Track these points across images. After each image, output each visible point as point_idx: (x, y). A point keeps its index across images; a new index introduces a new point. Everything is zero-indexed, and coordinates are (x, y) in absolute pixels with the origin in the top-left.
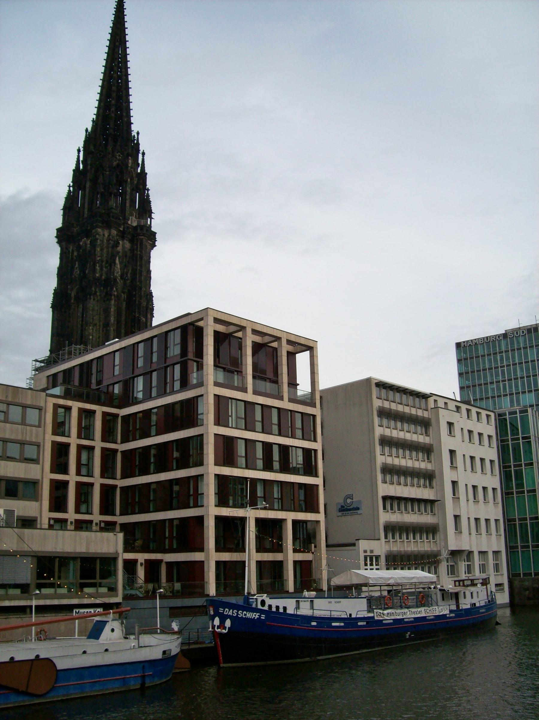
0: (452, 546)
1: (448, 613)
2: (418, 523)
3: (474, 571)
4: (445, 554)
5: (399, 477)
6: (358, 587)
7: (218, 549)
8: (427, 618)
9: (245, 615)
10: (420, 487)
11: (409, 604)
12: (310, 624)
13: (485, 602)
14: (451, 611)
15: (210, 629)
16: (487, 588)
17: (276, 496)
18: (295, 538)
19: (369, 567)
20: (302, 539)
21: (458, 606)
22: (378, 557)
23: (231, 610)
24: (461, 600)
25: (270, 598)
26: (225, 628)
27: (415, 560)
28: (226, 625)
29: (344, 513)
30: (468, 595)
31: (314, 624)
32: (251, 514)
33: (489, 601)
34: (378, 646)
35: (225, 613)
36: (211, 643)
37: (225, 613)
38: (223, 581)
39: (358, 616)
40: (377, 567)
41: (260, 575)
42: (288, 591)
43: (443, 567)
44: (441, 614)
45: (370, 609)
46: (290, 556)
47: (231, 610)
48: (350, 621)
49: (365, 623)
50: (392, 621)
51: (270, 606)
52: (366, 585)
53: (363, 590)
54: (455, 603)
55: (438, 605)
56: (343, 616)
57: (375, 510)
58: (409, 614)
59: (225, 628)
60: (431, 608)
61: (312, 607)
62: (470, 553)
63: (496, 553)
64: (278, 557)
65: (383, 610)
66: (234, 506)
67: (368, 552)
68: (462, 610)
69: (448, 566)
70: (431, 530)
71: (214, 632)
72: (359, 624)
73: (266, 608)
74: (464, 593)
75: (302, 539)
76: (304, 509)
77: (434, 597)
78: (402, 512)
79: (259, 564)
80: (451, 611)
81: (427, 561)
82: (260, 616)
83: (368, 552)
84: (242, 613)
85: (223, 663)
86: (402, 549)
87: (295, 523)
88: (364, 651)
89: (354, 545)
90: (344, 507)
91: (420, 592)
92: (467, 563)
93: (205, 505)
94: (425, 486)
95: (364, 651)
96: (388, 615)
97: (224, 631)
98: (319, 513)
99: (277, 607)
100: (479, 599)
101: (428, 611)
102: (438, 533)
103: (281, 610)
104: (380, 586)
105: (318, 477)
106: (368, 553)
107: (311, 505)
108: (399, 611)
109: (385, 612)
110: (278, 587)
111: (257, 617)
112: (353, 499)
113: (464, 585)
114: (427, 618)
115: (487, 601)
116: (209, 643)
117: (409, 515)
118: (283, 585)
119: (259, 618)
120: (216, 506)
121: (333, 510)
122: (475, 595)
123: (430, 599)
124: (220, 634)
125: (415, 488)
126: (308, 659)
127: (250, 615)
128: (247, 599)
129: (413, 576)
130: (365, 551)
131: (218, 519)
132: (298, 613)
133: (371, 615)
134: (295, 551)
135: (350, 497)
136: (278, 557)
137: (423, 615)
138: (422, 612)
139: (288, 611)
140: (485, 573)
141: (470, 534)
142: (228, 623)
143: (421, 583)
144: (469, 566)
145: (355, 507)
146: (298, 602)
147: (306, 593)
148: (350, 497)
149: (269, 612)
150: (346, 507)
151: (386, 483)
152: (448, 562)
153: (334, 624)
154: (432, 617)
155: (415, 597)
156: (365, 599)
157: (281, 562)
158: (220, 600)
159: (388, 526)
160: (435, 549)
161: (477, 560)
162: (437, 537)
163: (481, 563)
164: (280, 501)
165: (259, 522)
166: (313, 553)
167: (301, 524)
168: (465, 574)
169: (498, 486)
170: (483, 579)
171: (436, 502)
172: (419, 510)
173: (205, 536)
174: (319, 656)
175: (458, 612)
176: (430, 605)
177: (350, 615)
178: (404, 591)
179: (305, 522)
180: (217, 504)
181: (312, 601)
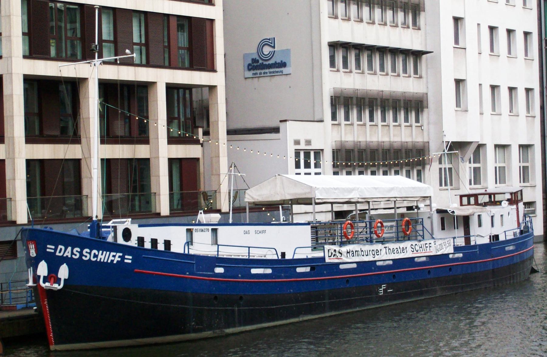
1: (452, 252)
2: (390, 92)
3: (486, 180)
5: (359, 7)
6: (287, 205)
7: (30, 139)
8: (416, 259)
9: (96, 256)
10: (397, 26)
11: (384, 235)
12: (213, 271)
13: (515, 234)
14: (457, 249)
15: (31, 283)
16: (517, 209)
17: (136, 39)
18: (170, 120)
19: (302, 170)
20: (182, 119)
21: (468, 240)
22: (318, 153)
23: (69, 249)
24: (474, 229)
25: (140, 226)
26: (58, 281)
27: (384, 159)
28: (59, 276)
29: (258, 72)
30: (486, 220)
31: (219, 270)
32: (93, 72)
33: (521, 232)
34: (331, 310)
35: (57, 254)
36: (27, 308)
37: (57, 254)
38: (38, 197)
40: (318, 170)
41: (108, 187)
42: (159, 214)
43: (432, 172)
45: (317, 245)
46: (161, 151)
48: (283, 265)
49: (308, 269)
50: (355, 266)
51: (141, 240)
52: (307, 201)
53: (294, 212)
54: (462, 234)
55: (433, 238)
56: (269, 257)
58: (385, 253)
59: (57, 281)
60: (422, 243)
61: (215, 242)
62: (480, 146)
63: (525, 148)
64: (141, 151)
65: (341, 246)
66: (58, 58)
67: (303, 143)
68: (475, 246)
69: (440, 169)
70: (414, 106)
71: (37, 289)
72: (299, 270)
73: (133, 242)
74: (479, 216)
75: (182, 119)
76: (187, 64)
78: (363, 73)
79: (108, 165)
80: (457, 249)
81: (408, 159)
82: (123, 258)
83: (303, 143)
84: (90, 253)
85: (56, 343)
86: (362, 139)
87: (171, 88)
88: (306, 318)
89: (276, 130)
90: (258, 61)
91: (402, 215)
92: (473, 165)
93: (4, 55)
94: (405, 25)
95: (306, 318)
96: (346, 256)
97: (56, 286)
98: (215, 71)
99: (154, 242)
100: (505, 228)
101: (417, 248)
102: (426, 110)
103: (161, 247)
104: (332, 203)
105: (213, 5)
106: (303, 146)
107: (201, 59)
108: (367, 247)
109: (344, 249)
110: (140, 207)
111: (117, 259)
112: (274, 47)
113: (477, 203)
114: (416, 259)
115: (518, 231)
116: (23, 309)
117: (375, 78)
118: (148, 202)
119: (122, 261)
120: (25, 57)
121: (240, 66)
122: (497, 220)
123: (419, 227)
124: (50, 292)
125: (399, 30)
126: (208, 334)
127: (104, 256)
128: (96, 226)
129: (392, 186)
130: (297, 142)
131: (30, 81)
132: (192, 252)
133: (318, 254)
134: (172, 140)
135: (270, 42)
136: (141, 151)
138: (407, 250)
139: (174, 249)
140: (505, 183)
142: (64, 272)
143: (404, 199)
144: (476, 171)
145: (279, 61)
146: (189, 231)
147: (202, 217)
148: (270, 42)
149: (138, 251)
150: (261, 61)
151: (336, 18)
152: (440, 163)
153: (254, 271)
154: (424, 259)
155: (394, 224)
156: (309, 227)
157: (77, 162)
158: (48, 229)
159: (339, 97)
161: (491, 159)
162: (425, 117)
163: (498, 165)
164: (144, 48)
165: (107, 88)
166: (202, 145)
167: (181, 91)
168: (470, 184)
169: (534, 28)
170: (511, 194)
171: (424, 56)
172: (394, 70)
173: (6, 113)
174: (229, 327)
175: (468, 249)
176: (419, 238)
177: (283, 254)
178: (373, 212)
179: (188, 88)
180: (27, 54)
181: (215, 231)
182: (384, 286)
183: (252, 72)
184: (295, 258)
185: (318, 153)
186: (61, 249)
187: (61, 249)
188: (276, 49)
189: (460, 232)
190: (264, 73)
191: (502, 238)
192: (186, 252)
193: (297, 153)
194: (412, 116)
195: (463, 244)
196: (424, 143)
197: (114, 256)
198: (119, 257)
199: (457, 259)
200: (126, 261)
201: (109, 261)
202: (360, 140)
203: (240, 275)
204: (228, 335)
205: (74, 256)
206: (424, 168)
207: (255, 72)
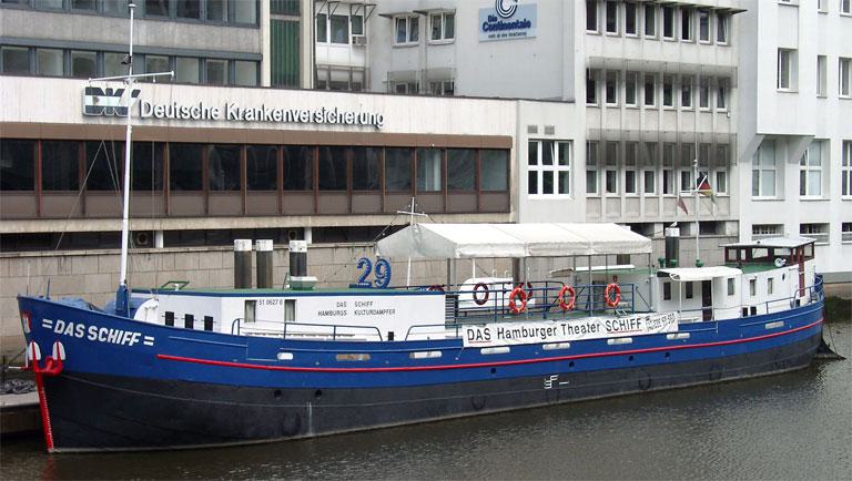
0: (767, 126)
2: (680, 64)
4: (743, 146)
9: (104, 335)
21: (707, 314)
22: (564, 146)
23: (71, 324)
29: (496, 33)
31: (288, 356)
35: (56, 331)
37: (56, 331)
39: (410, 338)
44: (652, 332)
47: (71, 324)
48: (392, 351)
54: (700, 306)
57: (565, 29)
70: (719, 86)
77: (643, 290)
82: (141, 339)
84: (98, 332)
90: (495, 19)
99: (189, 319)
103: (199, 326)
106: (541, 135)
127: (118, 337)
130: (532, 129)
133: (452, 334)
137: (601, 334)
141: (822, 97)
150: (499, 20)
160: (724, 130)
162: (735, 99)
175: (707, 329)
177: (391, 335)
182: (553, 378)
183: (489, 33)
184: (408, 339)
185: (564, 146)
186: (60, 325)
187: (60, 325)
188: (518, 3)
189: (697, 302)
190: (503, 35)
191: (761, 311)
192: (235, 333)
193: (533, 146)
194: (714, 99)
195: (701, 320)
196: (730, 135)
197: (129, 336)
198: (137, 337)
199: (681, 341)
200: (145, 343)
201: (123, 343)
202: (630, 128)
203: (318, 363)
204: (296, 440)
205: (83, 327)
206: (729, 169)
207: (492, 33)
